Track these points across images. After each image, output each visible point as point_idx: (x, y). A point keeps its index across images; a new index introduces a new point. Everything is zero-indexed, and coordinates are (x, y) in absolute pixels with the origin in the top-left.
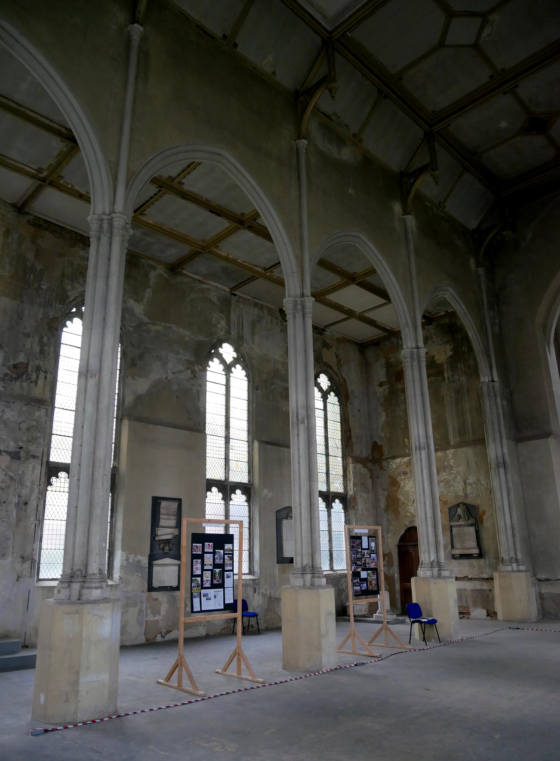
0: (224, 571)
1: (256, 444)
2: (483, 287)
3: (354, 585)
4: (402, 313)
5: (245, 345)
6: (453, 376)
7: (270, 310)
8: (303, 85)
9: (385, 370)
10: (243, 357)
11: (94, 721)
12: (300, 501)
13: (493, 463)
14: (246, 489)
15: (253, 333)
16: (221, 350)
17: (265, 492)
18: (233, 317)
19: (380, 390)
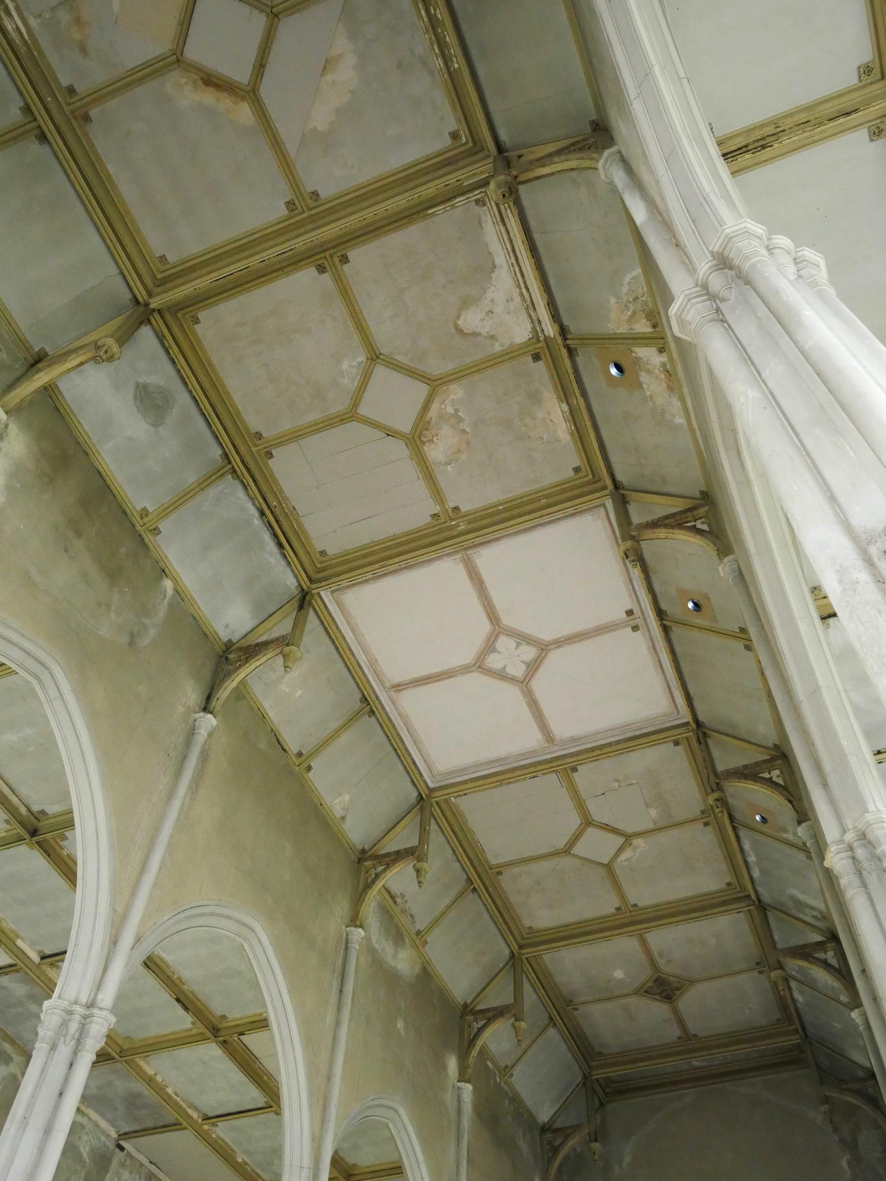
8: (374, 846)
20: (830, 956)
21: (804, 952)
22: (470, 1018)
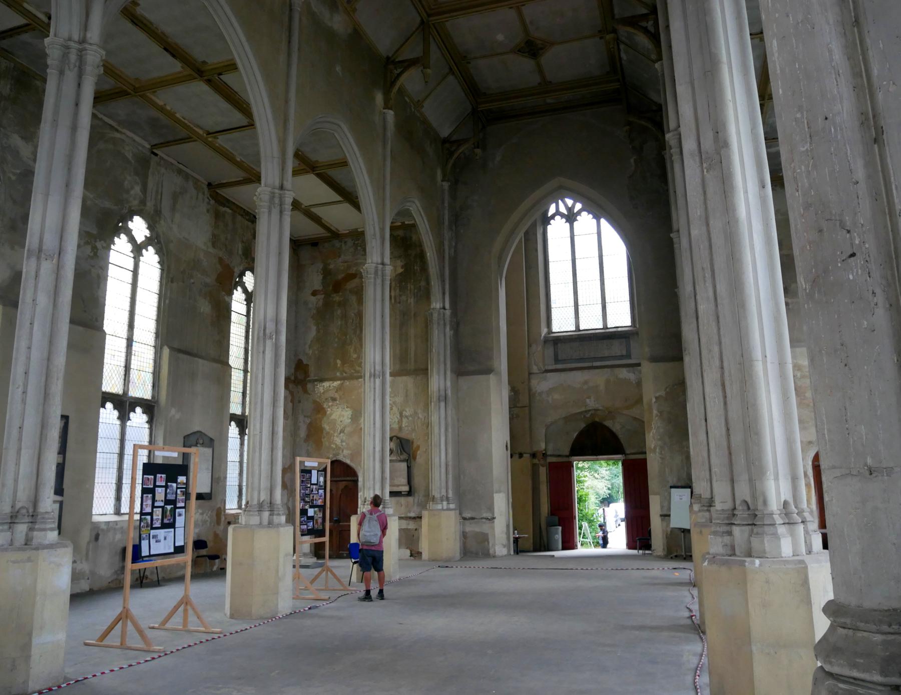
0: (176, 508)
1: (166, 351)
2: (446, 205)
3: (301, 523)
4: (374, 219)
5: (162, 222)
6: (400, 296)
7: (196, 182)
9: (321, 277)
10: (158, 237)
11: (50, 689)
12: (261, 428)
13: (435, 395)
14: (149, 407)
15: (173, 209)
16: (130, 225)
17: (173, 411)
18: (151, 184)
19: (313, 299)
20: (650, 25)
21: (633, 21)
22: (391, 67)
